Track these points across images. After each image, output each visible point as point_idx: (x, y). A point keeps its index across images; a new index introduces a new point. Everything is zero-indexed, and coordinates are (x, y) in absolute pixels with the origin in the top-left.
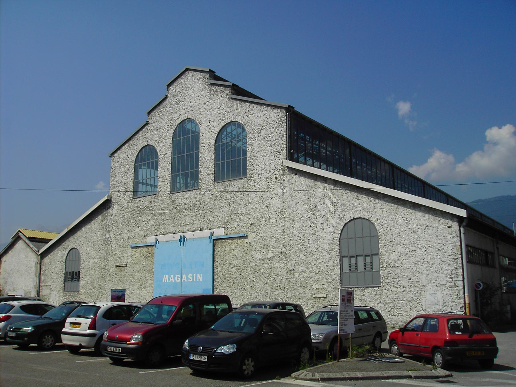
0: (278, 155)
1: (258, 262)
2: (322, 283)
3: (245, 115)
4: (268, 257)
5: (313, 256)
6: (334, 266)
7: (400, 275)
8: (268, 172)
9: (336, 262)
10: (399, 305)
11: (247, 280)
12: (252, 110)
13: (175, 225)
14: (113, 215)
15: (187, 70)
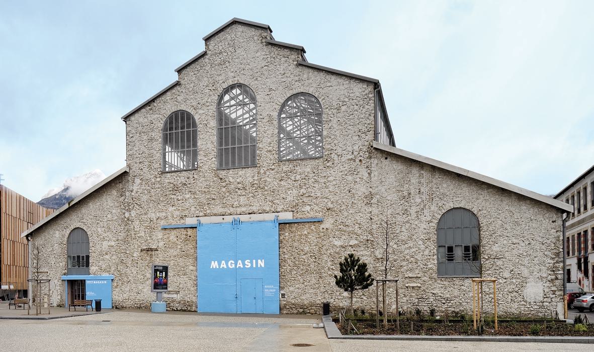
0: (363, 135)
1: (338, 249)
2: (417, 272)
3: (319, 87)
4: (350, 244)
5: (406, 245)
6: (430, 256)
7: (502, 267)
8: (350, 153)
9: (432, 252)
10: (500, 295)
11: (323, 268)
12: (330, 82)
13: (224, 206)
14: (134, 191)
15: (235, 22)
